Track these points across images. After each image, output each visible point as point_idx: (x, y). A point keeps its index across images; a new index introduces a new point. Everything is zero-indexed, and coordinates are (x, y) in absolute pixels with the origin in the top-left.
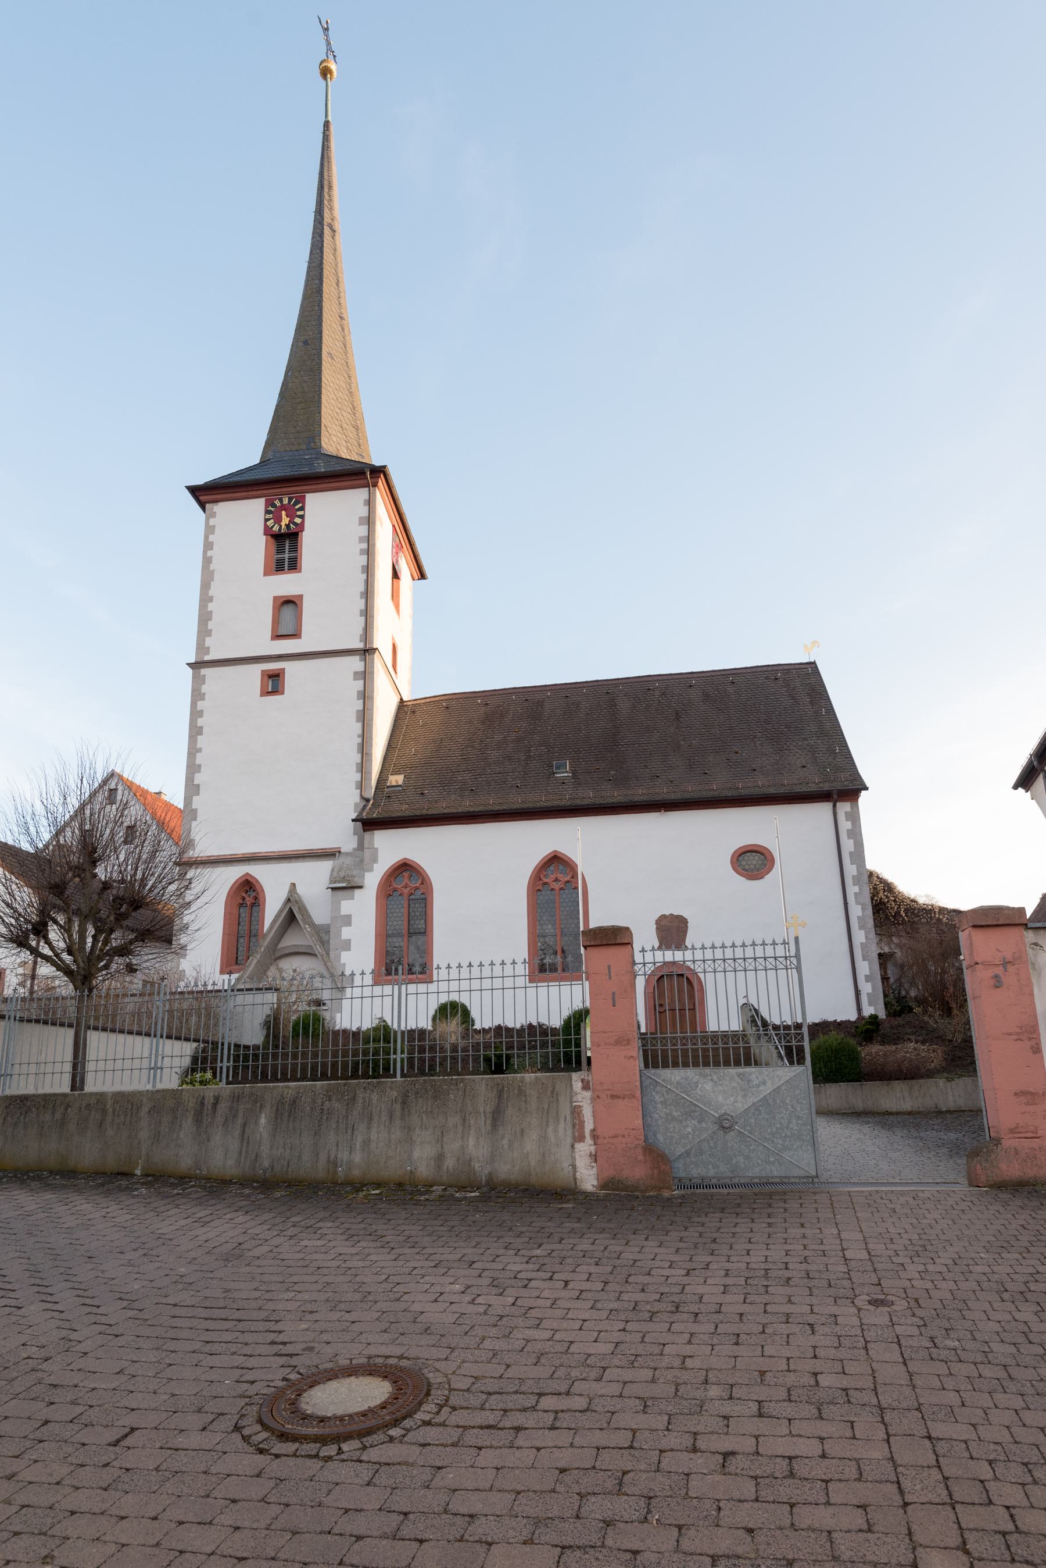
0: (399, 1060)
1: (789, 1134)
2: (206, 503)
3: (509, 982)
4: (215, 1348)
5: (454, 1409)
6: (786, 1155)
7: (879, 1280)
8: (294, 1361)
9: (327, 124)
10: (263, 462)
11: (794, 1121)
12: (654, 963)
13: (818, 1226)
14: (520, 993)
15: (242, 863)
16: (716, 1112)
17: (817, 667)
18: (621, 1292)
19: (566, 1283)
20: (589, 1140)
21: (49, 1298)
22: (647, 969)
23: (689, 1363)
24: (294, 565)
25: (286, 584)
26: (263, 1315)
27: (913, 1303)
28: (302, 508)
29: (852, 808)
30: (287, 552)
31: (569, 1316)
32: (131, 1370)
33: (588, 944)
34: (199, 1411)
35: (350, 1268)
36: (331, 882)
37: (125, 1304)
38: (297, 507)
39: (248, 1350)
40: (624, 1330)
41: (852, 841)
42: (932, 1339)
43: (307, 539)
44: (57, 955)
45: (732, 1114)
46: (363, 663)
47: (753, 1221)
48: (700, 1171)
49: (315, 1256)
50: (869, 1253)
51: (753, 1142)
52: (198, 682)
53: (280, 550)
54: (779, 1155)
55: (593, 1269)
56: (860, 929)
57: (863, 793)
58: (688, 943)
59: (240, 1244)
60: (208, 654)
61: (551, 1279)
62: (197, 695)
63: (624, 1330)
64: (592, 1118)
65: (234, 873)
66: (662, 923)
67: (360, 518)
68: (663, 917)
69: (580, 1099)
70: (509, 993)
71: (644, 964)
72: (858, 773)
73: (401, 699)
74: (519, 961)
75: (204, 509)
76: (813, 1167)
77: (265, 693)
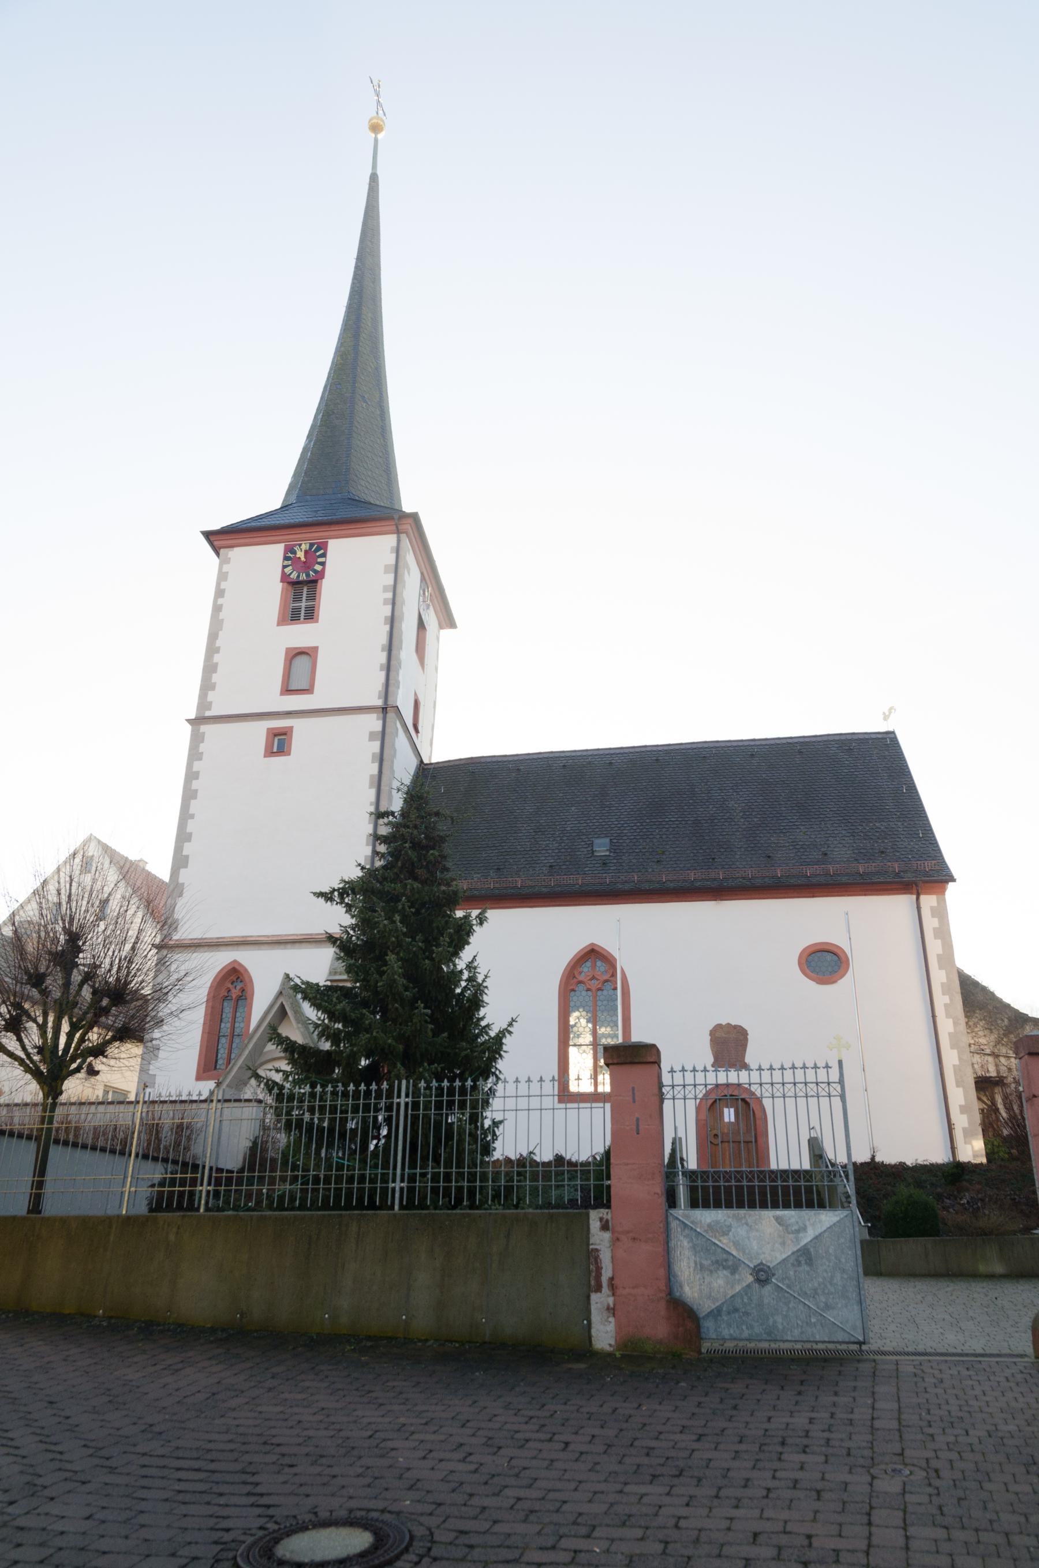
0: (397, 1189)
1: (833, 1290)
2: (220, 548)
3: (535, 1103)
4: (188, 1497)
5: (435, 1559)
6: (830, 1316)
7: (903, 1449)
8: (271, 1511)
9: (374, 179)
10: (284, 507)
11: (838, 1275)
12: (706, 1085)
13: (853, 1394)
14: (547, 1115)
15: (230, 948)
16: (751, 1261)
17: (896, 738)
18: (624, 1456)
19: (567, 1444)
20: (605, 1289)
21: (10, 1443)
22: (698, 1091)
23: (683, 1523)
24: (311, 615)
25: (300, 635)
26: (238, 1467)
27: (933, 1474)
28: (324, 555)
29: (938, 902)
30: (304, 600)
31: (565, 1477)
32: (100, 1516)
33: (611, 1062)
34: (173, 1555)
35: (333, 1423)
36: (330, 973)
37: (91, 1451)
38: (318, 554)
39: (222, 1501)
40: (621, 1492)
41: (939, 942)
42: (940, 1508)
43: (326, 587)
44: (28, 1055)
45: (769, 1264)
46: (380, 722)
47: (782, 1388)
48: (732, 1332)
49: (296, 1410)
50: (900, 1423)
51: (792, 1299)
52: (197, 739)
53: (297, 598)
54: (821, 1315)
55: (597, 1431)
56: (952, 1048)
57: (950, 884)
58: (748, 1059)
59: (214, 1394)
60: (210, 709)
61: (550, 1440)
62: (195, 754)
63: (621, 1492)
64: (611, 1265)
65: (220, 960)
66: (718, 1034)
67: (386, 566)
68: (718, 1027)
69: (598, 1242)
70: (535, 1115)
71: (673, 1086)
72: (944, 862)
73: (422, 761)
74: (547, 1078)
75: (218, 554)
76: (860, 1331)
77: (270, 753)
